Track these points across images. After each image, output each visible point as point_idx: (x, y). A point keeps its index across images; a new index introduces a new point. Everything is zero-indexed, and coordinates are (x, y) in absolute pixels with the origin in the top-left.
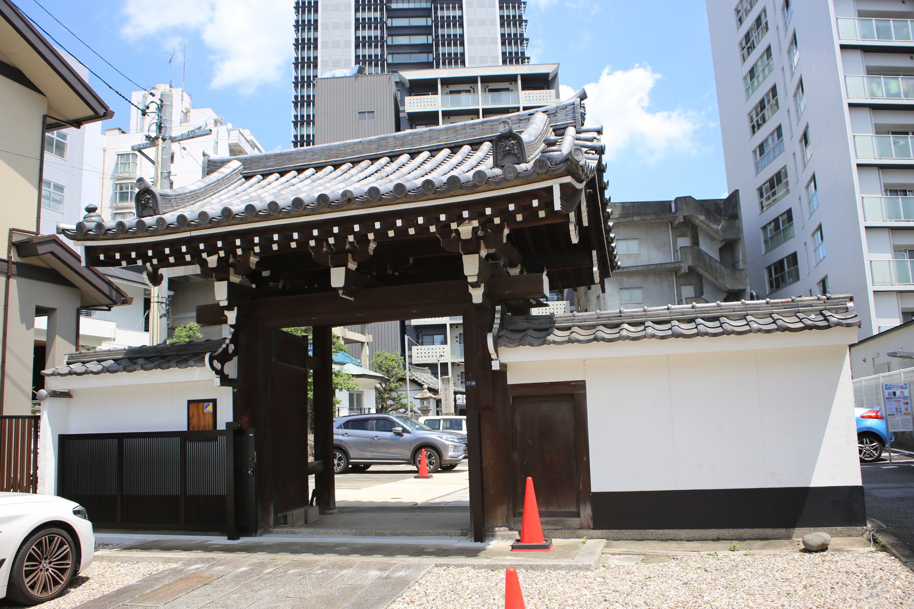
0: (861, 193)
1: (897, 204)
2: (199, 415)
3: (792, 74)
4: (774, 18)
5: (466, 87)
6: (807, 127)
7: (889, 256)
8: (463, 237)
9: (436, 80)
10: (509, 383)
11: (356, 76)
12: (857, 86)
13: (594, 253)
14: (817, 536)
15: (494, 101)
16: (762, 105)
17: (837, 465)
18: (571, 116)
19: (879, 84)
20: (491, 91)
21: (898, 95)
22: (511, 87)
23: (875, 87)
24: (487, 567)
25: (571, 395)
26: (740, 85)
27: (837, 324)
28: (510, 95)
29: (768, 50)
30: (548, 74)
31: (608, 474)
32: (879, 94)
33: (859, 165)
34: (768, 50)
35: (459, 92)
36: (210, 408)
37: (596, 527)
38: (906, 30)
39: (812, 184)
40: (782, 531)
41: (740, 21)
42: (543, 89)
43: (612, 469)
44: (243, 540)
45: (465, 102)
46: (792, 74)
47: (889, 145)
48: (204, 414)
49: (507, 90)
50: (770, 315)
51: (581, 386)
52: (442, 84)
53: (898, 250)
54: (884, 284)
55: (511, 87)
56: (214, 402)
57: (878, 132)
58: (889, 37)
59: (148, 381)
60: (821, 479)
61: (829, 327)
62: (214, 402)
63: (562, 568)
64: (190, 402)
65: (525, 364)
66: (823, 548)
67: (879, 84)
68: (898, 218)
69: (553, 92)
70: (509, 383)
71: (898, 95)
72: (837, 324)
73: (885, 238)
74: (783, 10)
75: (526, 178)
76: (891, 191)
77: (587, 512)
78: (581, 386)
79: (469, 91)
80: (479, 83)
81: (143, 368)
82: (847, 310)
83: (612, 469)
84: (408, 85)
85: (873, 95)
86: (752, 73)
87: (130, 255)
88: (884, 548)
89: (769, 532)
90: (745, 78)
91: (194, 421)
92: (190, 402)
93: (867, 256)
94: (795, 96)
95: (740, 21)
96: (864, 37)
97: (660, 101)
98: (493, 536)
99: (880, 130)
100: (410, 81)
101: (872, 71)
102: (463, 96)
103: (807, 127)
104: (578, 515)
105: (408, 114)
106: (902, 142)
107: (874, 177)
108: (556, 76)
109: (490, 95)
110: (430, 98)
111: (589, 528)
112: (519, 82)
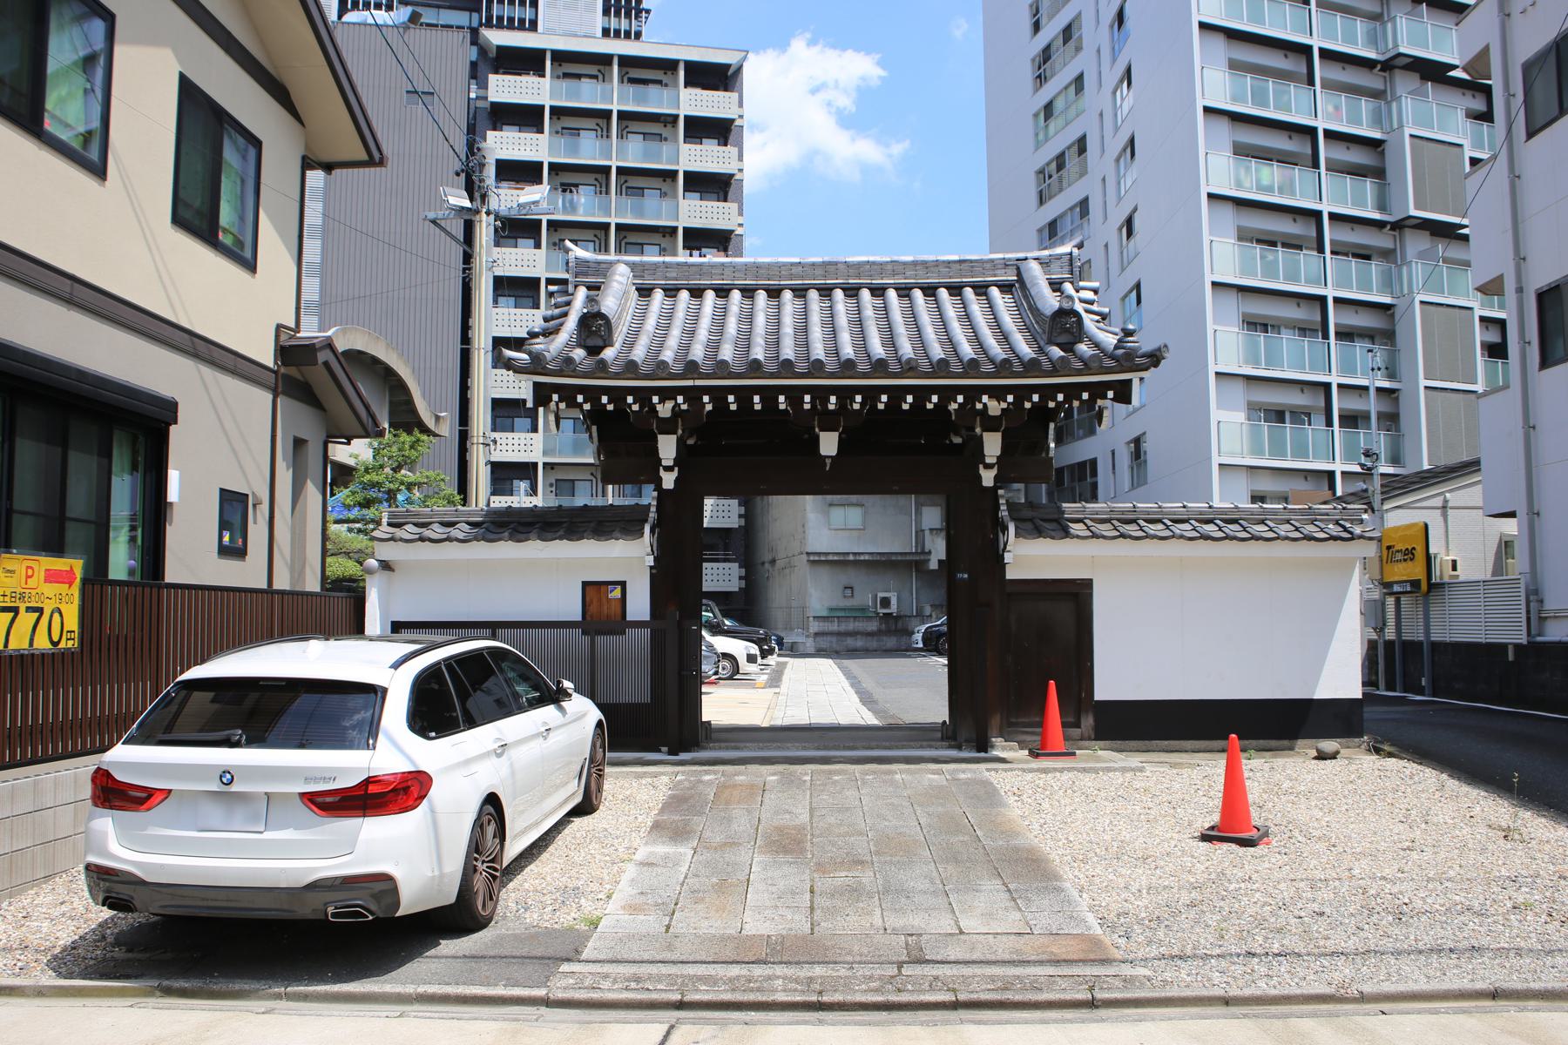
0: (1215, 322)
1: (1255, 346)
2: (600, 600)
3: (1117, 129)
4: (1095, 34)
5: (592, 70)
6: (1135, 209)
7: (1240, 416)
8: (991, 413)
9: (543, 51)
10: (1008, 577)
11: (405, 27)
12: (1221, 170)
13: (1052, 426)
14: (1329, 745)
15: (638, 101)
16: (1060, 161)
17: (1340, 676)
18: (1067, 268)
19: (1248, 169)
20: (633, 81)
21: (1269, 190)
22: (665, 79)
23: (1242, 172)
24: (1038, 770)
25: (1074, 598)
26: (1027, 125)
27: (1361, 537)
28: (666, 93)
29: (1079, 81)
30: (728, 66)
31: (1110, 685)
32: (1247, 184)
33: (1214, 284)
34: (1079, 81)
35: (579, 76)
36: (617, 593)
37: (1096, 739)
38: (1286, 98)
39: (1134, 294)
40: (1286, 743)
41: (1037, 27)
42: (716, 89)
43: (1117, 676)
44: (684, 756)
45: (587, 95)
46: (1117, 129)
47: (1254, 258)
48: (609, 600)
49: (659, 82)
50: (1288, 522)
51: (1087, 584)
52: (553, 60)
53: (1253, 408)
54: (1232, 454)
55: (665, 79)
56: (623, 584)
57: (1240, 239)
58: (1265, 105)
59: (542, 555)
60: (1326, 689)
61: (1352, 539)
62: (623, 584)
63: (1115, 770)
64: (585, 584)
65: (1029, 558)
66: (1333, 756)
67: (1248, 169)
68: (1256, 363)
69: (735, 95)
70: (1008, 577)
71: (1269, 190)
72: (1361, 537)
73: (1238, 391)
74: (1112, 26)
75: (1088, 366)
76: (1249, 323)
77: (1088, 722)
78: (1087, 584)
79: (595, 77)
80: (616, 68)
81: (511, 538)
82: (1362, 521)
83: (1117, 676)
84: (493, 54)
85: (1239, 185)
86: (1048, 109)
87: (816, 441)
88: (1390, 755)
89: (1273, 743)
90: (1036, 115)
91: (593, 609)
92: (585, 584)
93: (1216, 414)
94: (1118, 160)
95: (1037, 27)
96: (1234, 99)
97: (865, 113)
98: (993, 747)
99: (1244, 236)
100: (499, 48)
101: (1241, 151)
102: (586, 84)
103: (1135, 209)
104: (1078, 725)
105: (493, 104)
106: (1270, 257)
107: (1231, 301)
108: (740, 68)
109: (631, 89)
110: (529, 80)
111: (1090, 739)
112: (682, 73)
